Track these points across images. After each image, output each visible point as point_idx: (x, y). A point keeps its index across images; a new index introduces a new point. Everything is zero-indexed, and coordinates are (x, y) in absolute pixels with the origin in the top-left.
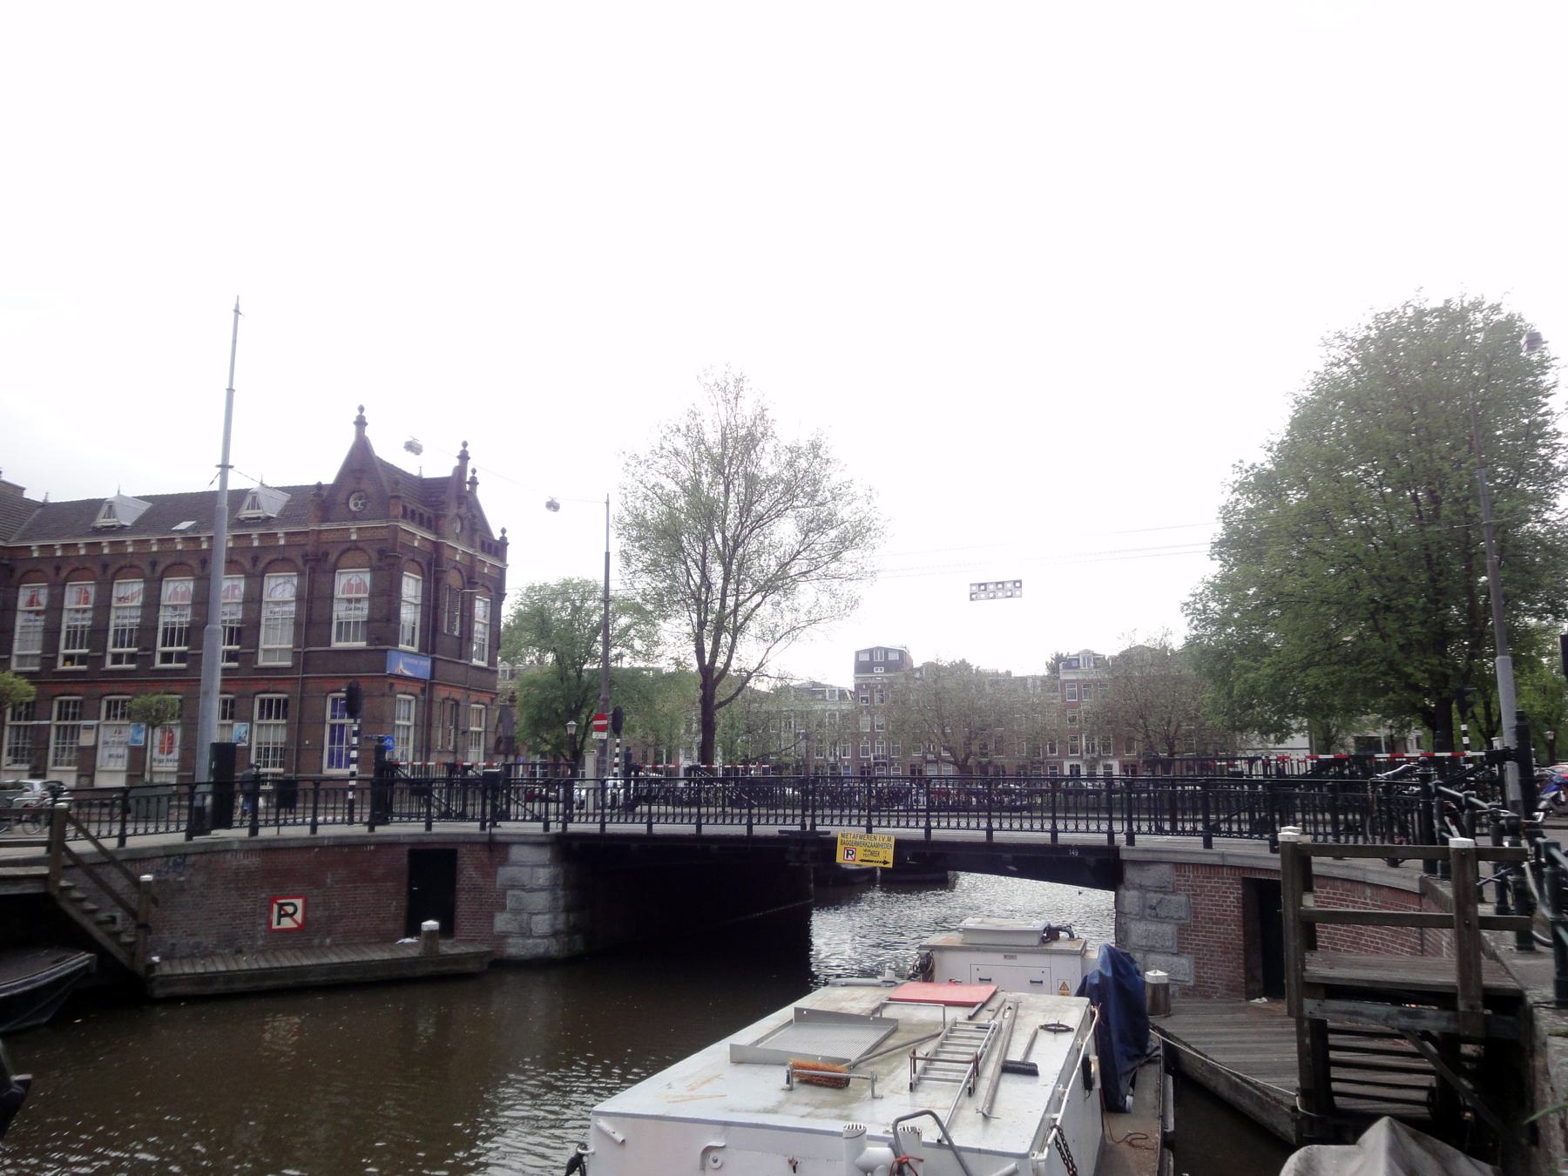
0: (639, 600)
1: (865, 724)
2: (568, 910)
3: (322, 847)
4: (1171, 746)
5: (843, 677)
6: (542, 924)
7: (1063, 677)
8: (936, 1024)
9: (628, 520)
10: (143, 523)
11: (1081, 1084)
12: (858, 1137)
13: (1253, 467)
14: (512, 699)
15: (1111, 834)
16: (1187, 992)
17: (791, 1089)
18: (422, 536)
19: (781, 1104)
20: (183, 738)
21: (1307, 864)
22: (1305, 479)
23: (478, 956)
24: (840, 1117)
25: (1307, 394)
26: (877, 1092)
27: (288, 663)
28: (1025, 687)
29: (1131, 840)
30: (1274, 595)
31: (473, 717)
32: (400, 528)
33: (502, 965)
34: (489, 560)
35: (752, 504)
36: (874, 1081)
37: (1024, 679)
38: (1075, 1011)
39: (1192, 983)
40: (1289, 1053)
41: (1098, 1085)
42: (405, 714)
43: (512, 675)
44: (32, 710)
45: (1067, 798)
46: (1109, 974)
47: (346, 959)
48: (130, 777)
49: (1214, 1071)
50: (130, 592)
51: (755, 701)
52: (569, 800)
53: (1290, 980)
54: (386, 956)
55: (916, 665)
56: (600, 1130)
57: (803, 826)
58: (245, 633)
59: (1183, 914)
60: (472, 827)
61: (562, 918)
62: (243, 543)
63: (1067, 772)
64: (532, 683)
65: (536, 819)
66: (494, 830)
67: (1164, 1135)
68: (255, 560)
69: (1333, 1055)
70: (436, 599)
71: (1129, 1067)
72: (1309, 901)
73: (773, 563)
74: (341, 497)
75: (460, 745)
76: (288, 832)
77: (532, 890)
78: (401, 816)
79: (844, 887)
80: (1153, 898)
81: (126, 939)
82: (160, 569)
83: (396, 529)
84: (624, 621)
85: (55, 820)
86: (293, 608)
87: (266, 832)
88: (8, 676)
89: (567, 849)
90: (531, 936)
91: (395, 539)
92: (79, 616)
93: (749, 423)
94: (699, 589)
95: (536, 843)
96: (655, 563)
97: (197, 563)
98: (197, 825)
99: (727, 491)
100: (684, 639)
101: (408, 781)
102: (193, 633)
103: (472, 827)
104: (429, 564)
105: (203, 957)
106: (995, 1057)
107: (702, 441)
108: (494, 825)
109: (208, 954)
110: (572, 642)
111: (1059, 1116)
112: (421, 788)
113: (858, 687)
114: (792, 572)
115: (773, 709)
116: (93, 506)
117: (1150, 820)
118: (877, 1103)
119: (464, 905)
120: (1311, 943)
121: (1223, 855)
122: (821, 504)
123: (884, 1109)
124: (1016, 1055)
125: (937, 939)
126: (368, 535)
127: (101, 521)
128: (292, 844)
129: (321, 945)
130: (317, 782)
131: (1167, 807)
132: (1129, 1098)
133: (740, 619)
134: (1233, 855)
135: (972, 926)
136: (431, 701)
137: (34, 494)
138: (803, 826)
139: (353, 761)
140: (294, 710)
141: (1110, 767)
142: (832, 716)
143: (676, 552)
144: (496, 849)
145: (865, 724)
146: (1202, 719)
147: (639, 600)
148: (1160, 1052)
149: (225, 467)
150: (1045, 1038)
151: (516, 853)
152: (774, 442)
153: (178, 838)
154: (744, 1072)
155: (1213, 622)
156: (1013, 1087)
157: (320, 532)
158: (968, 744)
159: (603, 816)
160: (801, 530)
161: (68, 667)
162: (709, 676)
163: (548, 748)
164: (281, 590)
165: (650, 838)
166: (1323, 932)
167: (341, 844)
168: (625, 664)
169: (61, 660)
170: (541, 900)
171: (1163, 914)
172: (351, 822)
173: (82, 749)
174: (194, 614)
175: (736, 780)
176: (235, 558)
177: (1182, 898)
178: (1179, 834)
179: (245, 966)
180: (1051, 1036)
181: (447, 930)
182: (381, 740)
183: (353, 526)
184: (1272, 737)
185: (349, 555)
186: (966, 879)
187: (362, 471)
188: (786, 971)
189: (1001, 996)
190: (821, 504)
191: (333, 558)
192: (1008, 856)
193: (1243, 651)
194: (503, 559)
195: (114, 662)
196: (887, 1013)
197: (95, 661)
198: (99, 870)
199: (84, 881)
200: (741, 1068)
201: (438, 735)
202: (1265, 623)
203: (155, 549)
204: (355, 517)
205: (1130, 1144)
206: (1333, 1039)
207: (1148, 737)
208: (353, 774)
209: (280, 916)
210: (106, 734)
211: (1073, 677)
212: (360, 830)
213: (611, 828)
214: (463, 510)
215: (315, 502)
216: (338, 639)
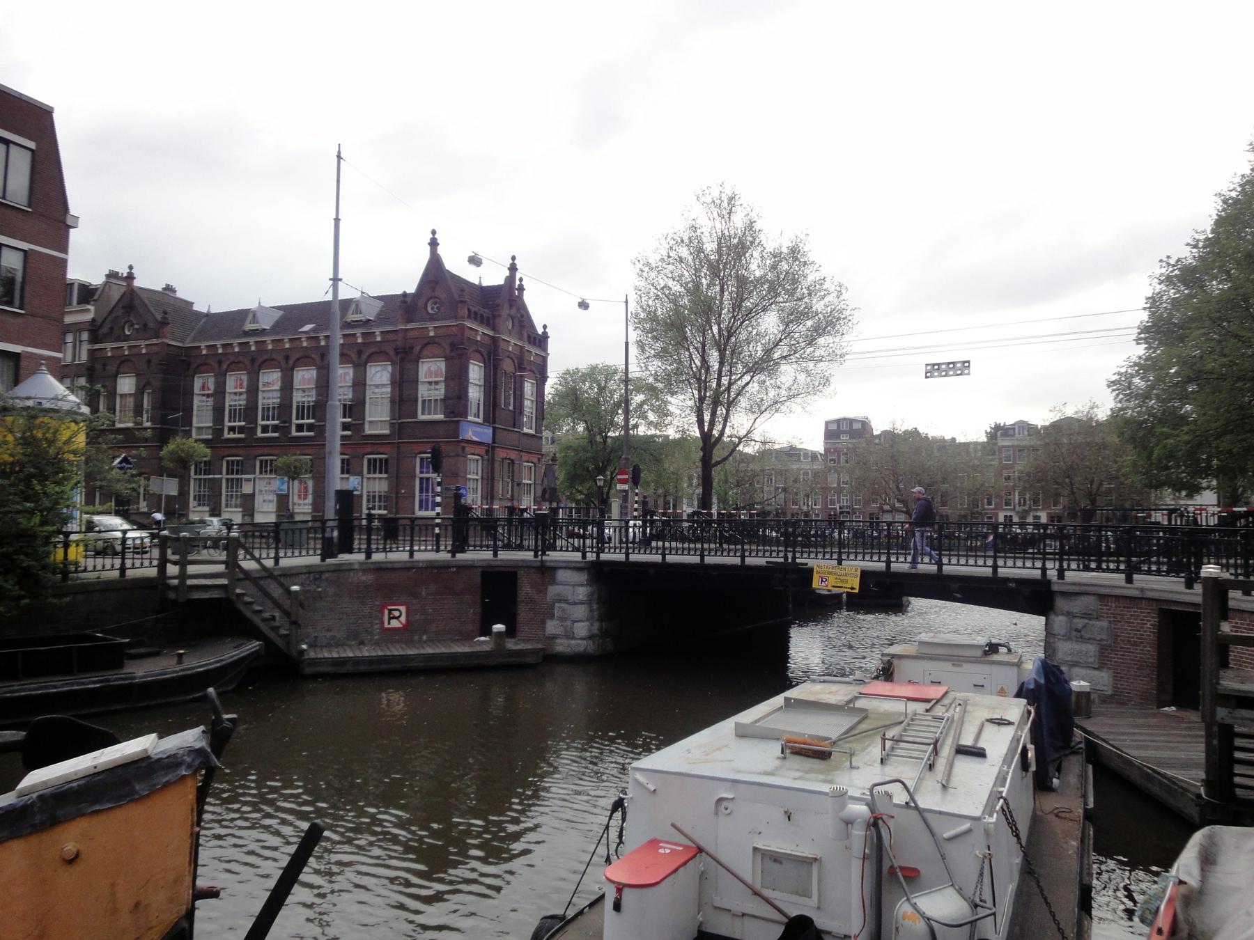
0: (651, 380)
1: (832, 480)
2: (601, 619)
4: (1093, 501)
5: (815, 442)
6: (582, 629)
8: (899, 714)
9: (642, 315)
10: (279, 326)
12: (841, 797)
13: (1179, 260)
14: (554, 459)
15: (1044, 570)
16: (1105, 700)
18: (482, 332)
19: (777, 768)
20: (315, 486)
21: (1225, 599)
23: (533, 652)
24: (825, 781)
25: (1234, 194)
26: (854, 764)
27: (387, 432)
28: (968, 452)
29: (1061, 575)
30: (1194, 373)
31: (525, 473)
32: (465, 324)
33: (549, 660)
34: (535, 350)
35: (742, 301)
36: (852, 755)
37: (966, 445)
38: (1015, 709)
39: (1109, 693)
40: (1198, 752)
41: (1033, 768)
42: (474, 470)
43: (553, 442)
44: (209, 467)
46: (1042, 681)
47: (438, 651)
48: (278, 516)
49: (1128, 763)
50: (271, 379)
51: (742, 461)
52: (600, 537)
53: (1205, 691)
54: (467, 649)
55: (876, 433)
56: (637, 781)
57: (786, 558)
58: (355, 409)
59: (1104, 637)
60: (529, 555)
61: (596, 625)
62: (351, 340)
63: (1001, 520)
64: (569, 448)
65: (576, 549)
66: (545, 558)
67: (1086, 810)
68: (360, 353)
69: (1237, 755)
70: (495, 380)
71: (1056, 756)
72: (1226, 627)
74: (421, 303)
75: (516, 494)
76: (393, 556)
77: (575, 604)
78: (475, 546)
79: (818, 608)
80: (1079, 623)
83: (462, 328)
84: (638, 398)
85: (232, 546)
86: (388, 389)
87: (377, 557)
88: (191, 442)
89: (599, 573)
90: (574, 638)
91: (463, 334)
92: (237, 398)
93: (740, 234)
95: (577, 568)
96: (665, 350)
97: (318, 357)
98: (329, 550)
99: (722, 290)
100: (688, 411)
101: (478, 519)
102: (319, 409)
103: (529, 555)
106: (949, 741)
107: (701, 250)
108: (544, 554)
109: (340, 645)
110: (599, 417)
111: (1005, 790)
112: (488, 525)
114: (776, 356)
116: (241, 315)
117: (1078, 560)
118: (854, 772)
119: (523, 614)
120: (1224, 664)
121: (1142, 590)
122: (800, 300)
123: (860, 778)
124: (967, 741)
125: (895, 650)
126: (441, 332)
127: (248, 326)
129: (420, 641)
130: (413, 520)
131: (1088, 552)
132: (1055, 781)
133: (733, 395)
134: (1151, 590)
135: (926, 639)
136: (493, 460)
137: (200, 307)
138: (786, 558)
139: (438, 505)
140: (393, 469)
141: (1039, 517)
142: (806, 473)
143: (682, 342)
144: (546, 572)
145: (832, 480)
146: (1122, 479)
147: (651, 380)
148: (1082, 745)
149: (336, 280)
150: (990, 729)
151: (562, 575)
152: (760, 249)
153: (315, 560)
154: (745, 743)
155: (1136, 397)
156: (965, 766)
159: (627, 548)
160: (782, 321)
161: (232, 436)
162: (708, 442)
163: (580, 497)
164: (380, 375)
165: (664, 565)
166: (1236, 651)
167: (432, 566)
168: (642, 430)
169: (226, 430)
170: (580, 611)
171: (1088, 636)
172: (438, 550)
173: (244, 496)
174: (318, 394)
175: (730, 522)
176: (345, 351)
177: (1105, 624)
178: (1103, 571)
179: (367, 654)
180: (996, 727)
181: (511, 632)
182: (458, 489)
183: (125, 344)
184: (1184, 493)
185: (429, 347)
186: (917, 603)
187: (436, 282)
188: (772, 674)
189: (952, 695)
190: (800, 300)
191: (417, 349)
192: (955, 586)
193: (1162, 422)
194: (545, 349)
196: (860, 704)
197: (283, 429)
198: (262, 582)
199: (252, 590)
200: (744, 741)
201: (499, 487)
202: (1185, 398)
203: (287, 346)
204: (432, 318)
206: (1238, 742)
207: (1073, 493)
208: (438, 514)
209: (390, 618)
210: (260, 485)
212: (444, 556)
213: (633, 558)
214: (513, 312)
215: (402, 307)
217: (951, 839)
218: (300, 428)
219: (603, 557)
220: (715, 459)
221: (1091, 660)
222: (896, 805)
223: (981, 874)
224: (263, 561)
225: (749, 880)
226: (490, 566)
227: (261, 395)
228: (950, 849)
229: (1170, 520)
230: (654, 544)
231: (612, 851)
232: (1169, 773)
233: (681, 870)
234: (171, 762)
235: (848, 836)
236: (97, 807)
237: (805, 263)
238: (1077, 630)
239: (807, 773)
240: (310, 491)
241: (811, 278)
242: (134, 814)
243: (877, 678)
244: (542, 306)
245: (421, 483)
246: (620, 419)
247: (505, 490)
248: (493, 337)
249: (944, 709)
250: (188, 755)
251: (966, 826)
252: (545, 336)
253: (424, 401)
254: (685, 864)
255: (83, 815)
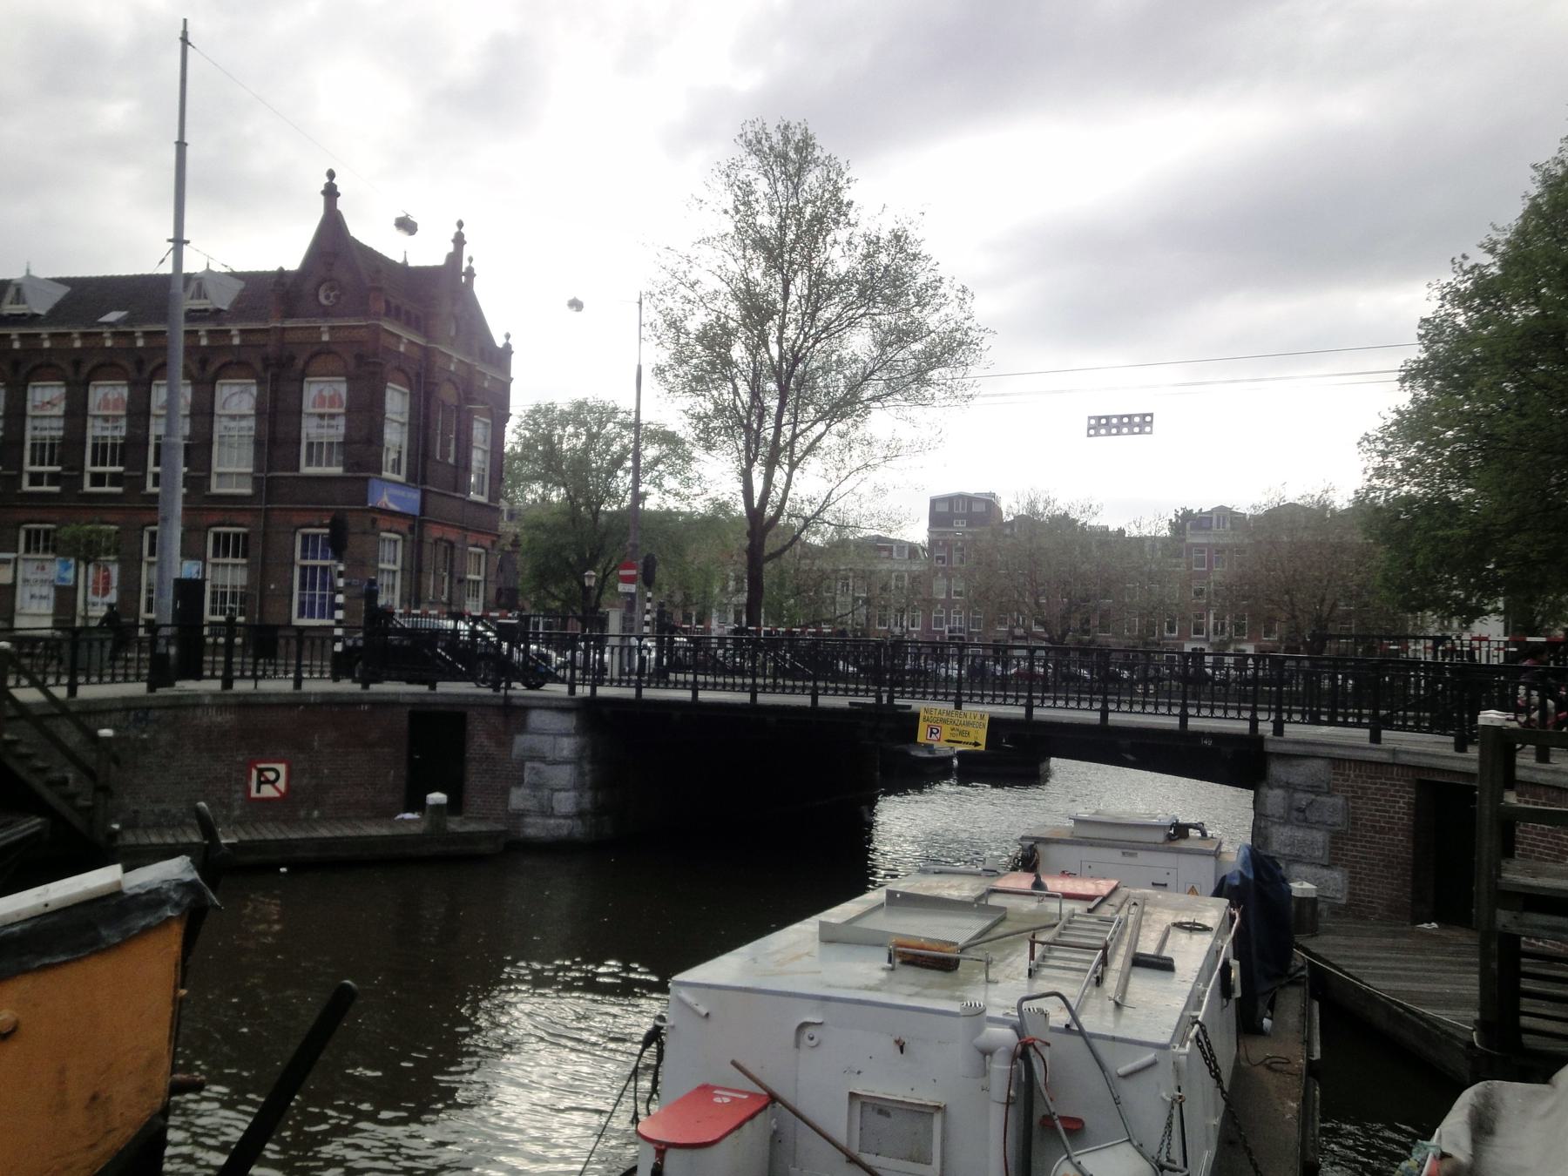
1: (939, 589)
2: (596, 787)
3: (307, 705)
6: (565, 802)
7: (1191, 540)
8: (1052, 915)
10: (59, 312)
11: (1218, 991)
12: (977, 1015)
14: (516, 543)
15: (1254, 722)
16: (1337, 911)
17: (892, 969)
19: (883, 982)
22: (1537, 290)
23: (491, 836)
24: (952, 998)
26: (991, 976)
27: (248, 491)
29: (1278, 729)
31: (471, 563)
32: (365, 330)
33: (513, 849)
37: (1140, 541)
38: (1213, 912)
39: (1344, 901)
41: (1238, 994)
42: (391, 559)
45: (1192, 682)
46: (1251, 876)
47: (338, 833)
49: (1370, 997)
54: (385, 831)
55: (926, 540)
56: (681, 1001)
58: (199, 450)
59: (1338, 819)
64: (539, 526)
67: (1310, 1063)
70: (427, 417)
73: (842, 383)
75: (455, 597)
76: (266, 686)
77: (555, 763)
79: (918, 774)
80: (1302, 799)
81: (81, 802)
82: (86, 369)
83: (377, 330)
86: (251, 423)
87: (240, 686)
89: (593, 714)
90: (552, 815)
94: (749, 413)
95: (559, 707)
98: (160, 674)
102: (132, 449)
104: (418, 375)
105: (171, 827)
106: (1123, 950)
113: (932, 542)
114: (866, 395)
115: (828, 567)
118: (991, 986)
119: (474, 778)
121: (1394, 752)
123: (1003, 990)
124: (1148, 947)
128: (274, 700)
134: (1408, 752)
138: (879, 699)
139: (339, 607)
142: (900, 578)
146: (1366, 598)
150: (1182, 937)
151: (537, 719)
153: (138, 689)
156: (1144, 986)
157: (284, 329)
158: (1065, 618)
164: (237, 400)
165: (695, 704)
166: (1527, 833)
168: (651, 504)
170: (564, 774)
171: (1314, 819)
177: (1339, 801)
181: (456, 805)
183: (324, 325)
189: (1124, 891)
191: (300, 363)
195: (32, 483)
196: (995, 900)
197: (70, 480)
198: (47, 723)
200: (833, 947)
203: (78, 344)
204: (326, 313)
205: (1269, 1067)
207: (1294, 617)
209: (260, 783)
211: (1203, 540)
216: (309, 464)
217: (1126, 1076)
218: (98, 479)
219: (602, 691)
220: (767, 551)
221: (1318, 853)
222: (1053, 1029)
223: (1169, 1125)
224: (53, 690)
225: (843, 1141)
226: (423, 704)
227: (29, 424)
228: (1128, 1090)
229: (1435, 657)
230: (672, 676)
231: (642, 1108)
232: (1429, 1012)
233: (748, 1125)
234: (152, 899)
235: (985, 1072)
236: (47, 961)
237: (915, 256)
238: (1300, 810)
239: (926, 987)
240: (115, 582)
241: (921, 280)
242: (99, 969)
243: (1014, 869)
244: (502, 306)
245: (303, 577)
246: (623, 480)
247: (438, 590)
248: (425, 349)
249: (1113, 910)
250: (175, 890)
251: (1150, 1056)
252: (507, 351)
253: (310, 445)
254: (752, 1117)
255: (26, 971)
